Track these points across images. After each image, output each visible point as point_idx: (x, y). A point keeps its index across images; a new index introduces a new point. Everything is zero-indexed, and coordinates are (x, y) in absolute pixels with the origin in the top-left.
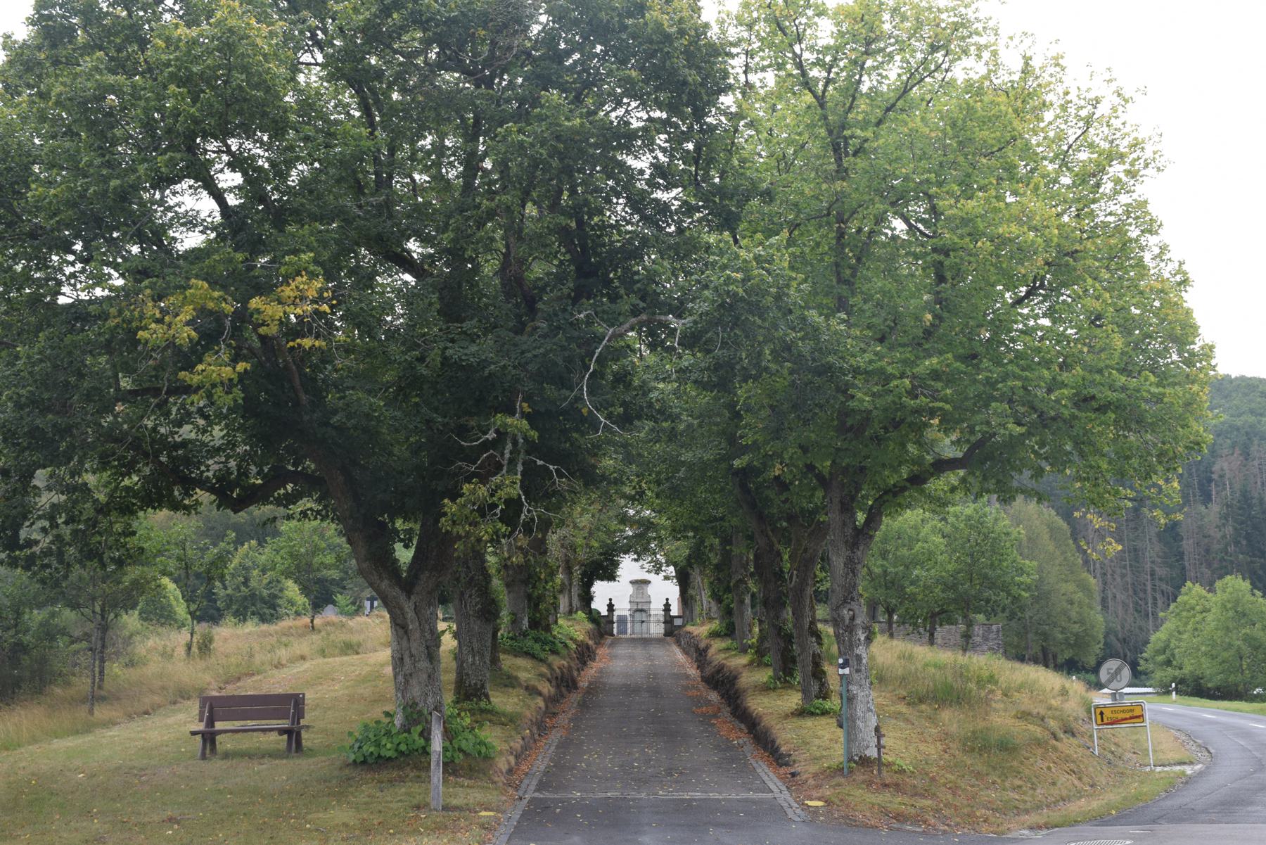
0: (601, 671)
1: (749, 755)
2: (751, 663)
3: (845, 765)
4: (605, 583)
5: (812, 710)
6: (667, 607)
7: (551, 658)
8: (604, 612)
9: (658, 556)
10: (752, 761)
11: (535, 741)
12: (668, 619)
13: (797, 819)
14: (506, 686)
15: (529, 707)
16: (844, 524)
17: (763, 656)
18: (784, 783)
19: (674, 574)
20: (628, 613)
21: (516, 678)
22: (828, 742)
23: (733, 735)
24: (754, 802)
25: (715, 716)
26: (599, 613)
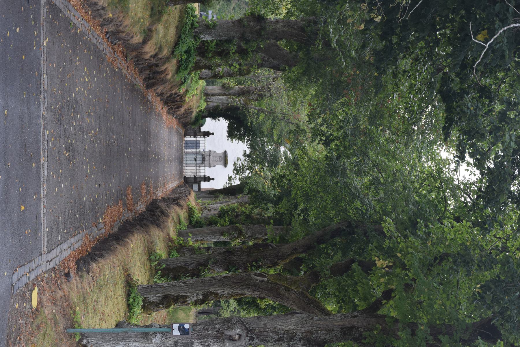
0: (159, 116)
1: (88, 232)
2: (170, 240)
3: (78, 330)
4: (226, 129)
5: (133, 295)
6: (207, 179)
7: (174, 61)
8: (203, 129)
9: (248, 171)
10: (82, 235)
11: (102, 26)
12: (198, 180)
13: (15, 278)
14: (152, 9)
15: (133, 25)
16: (330, 330)
17: (177, 251)
18: (58, 265)
19: (233, 184)
20: (201, 149)
21: (159, 20)
22: (101, 310)
23: (107, 219)
24: (36, 231)
25: (125, 205)
26: (202, 125)
